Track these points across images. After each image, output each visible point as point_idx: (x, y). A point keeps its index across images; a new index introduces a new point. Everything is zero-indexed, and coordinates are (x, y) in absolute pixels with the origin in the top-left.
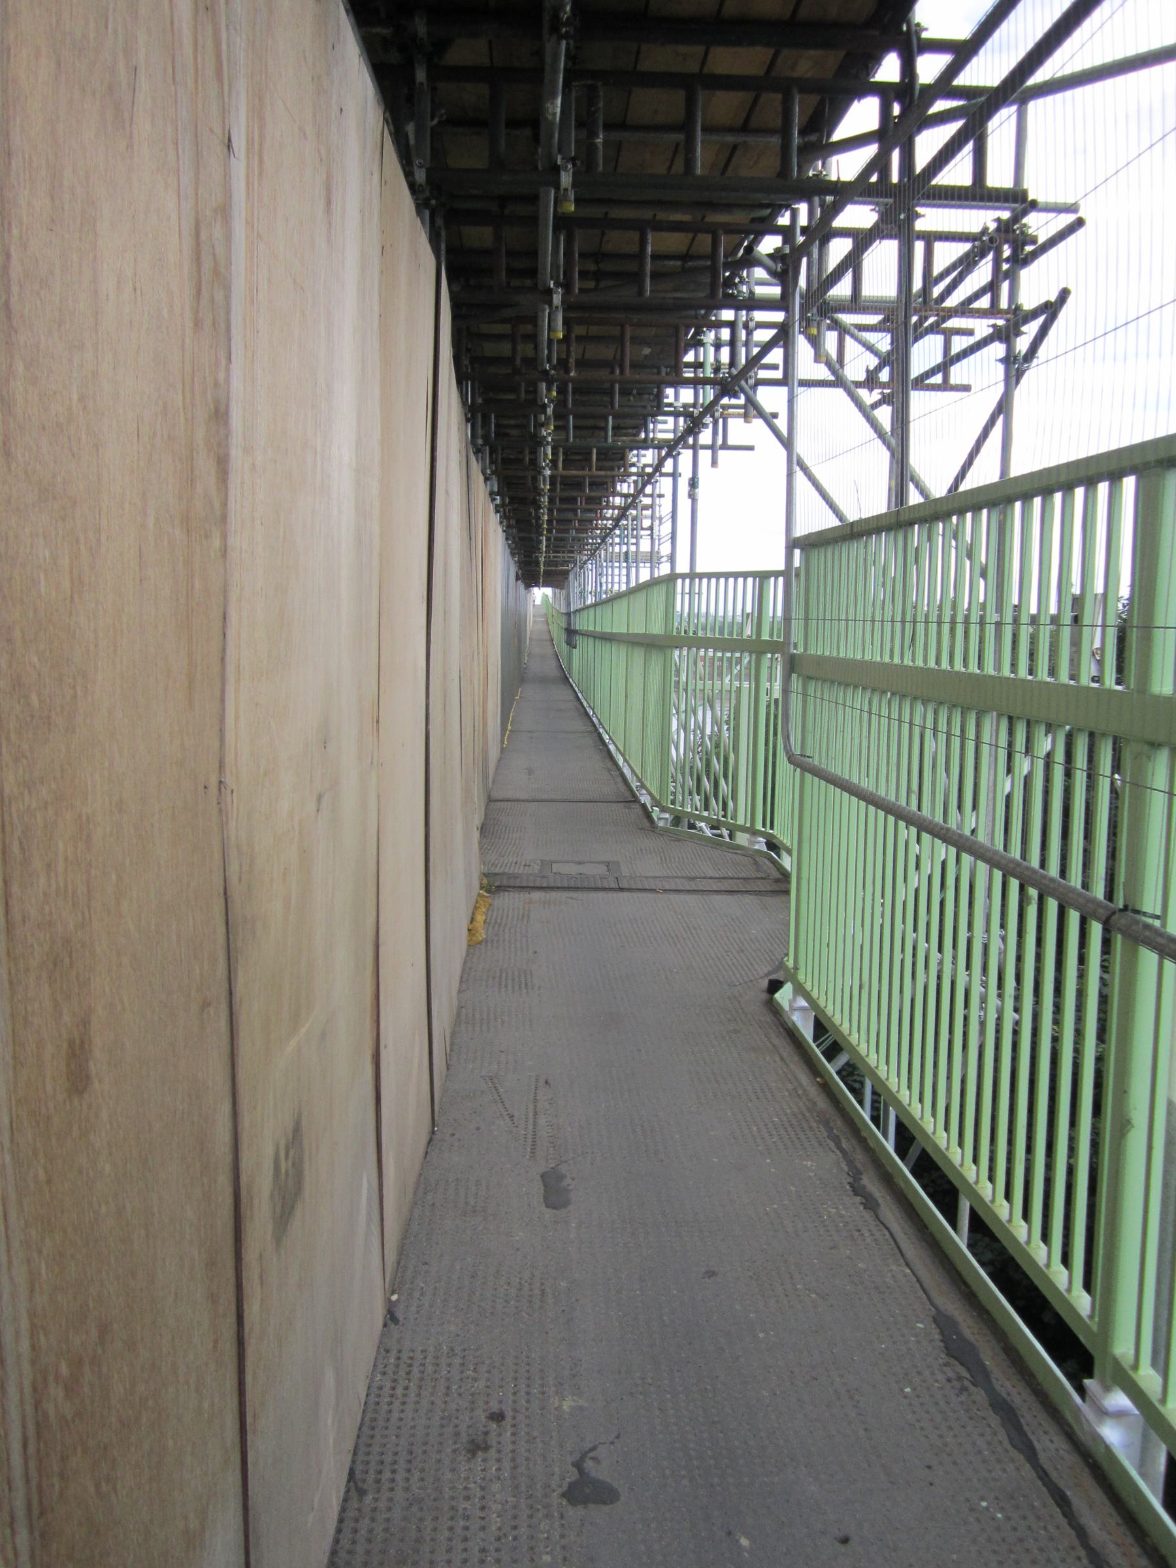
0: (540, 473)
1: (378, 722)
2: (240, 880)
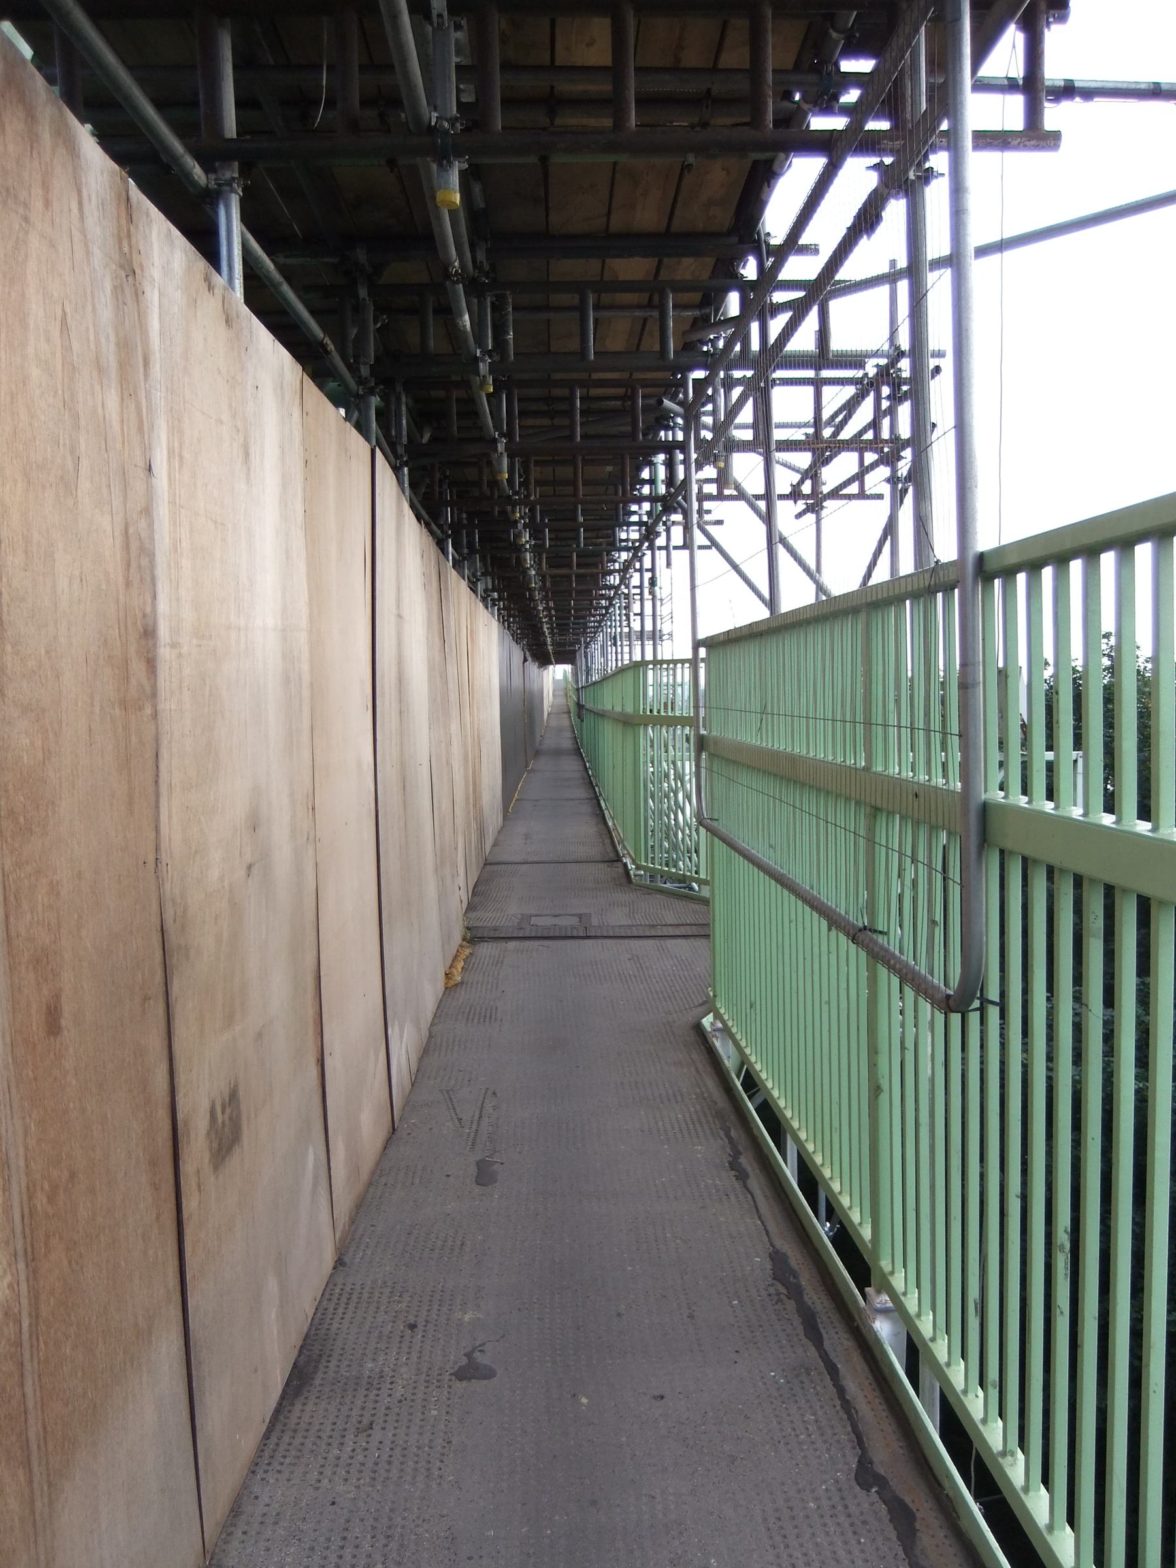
1: (313, 809)
2: (175, 921)
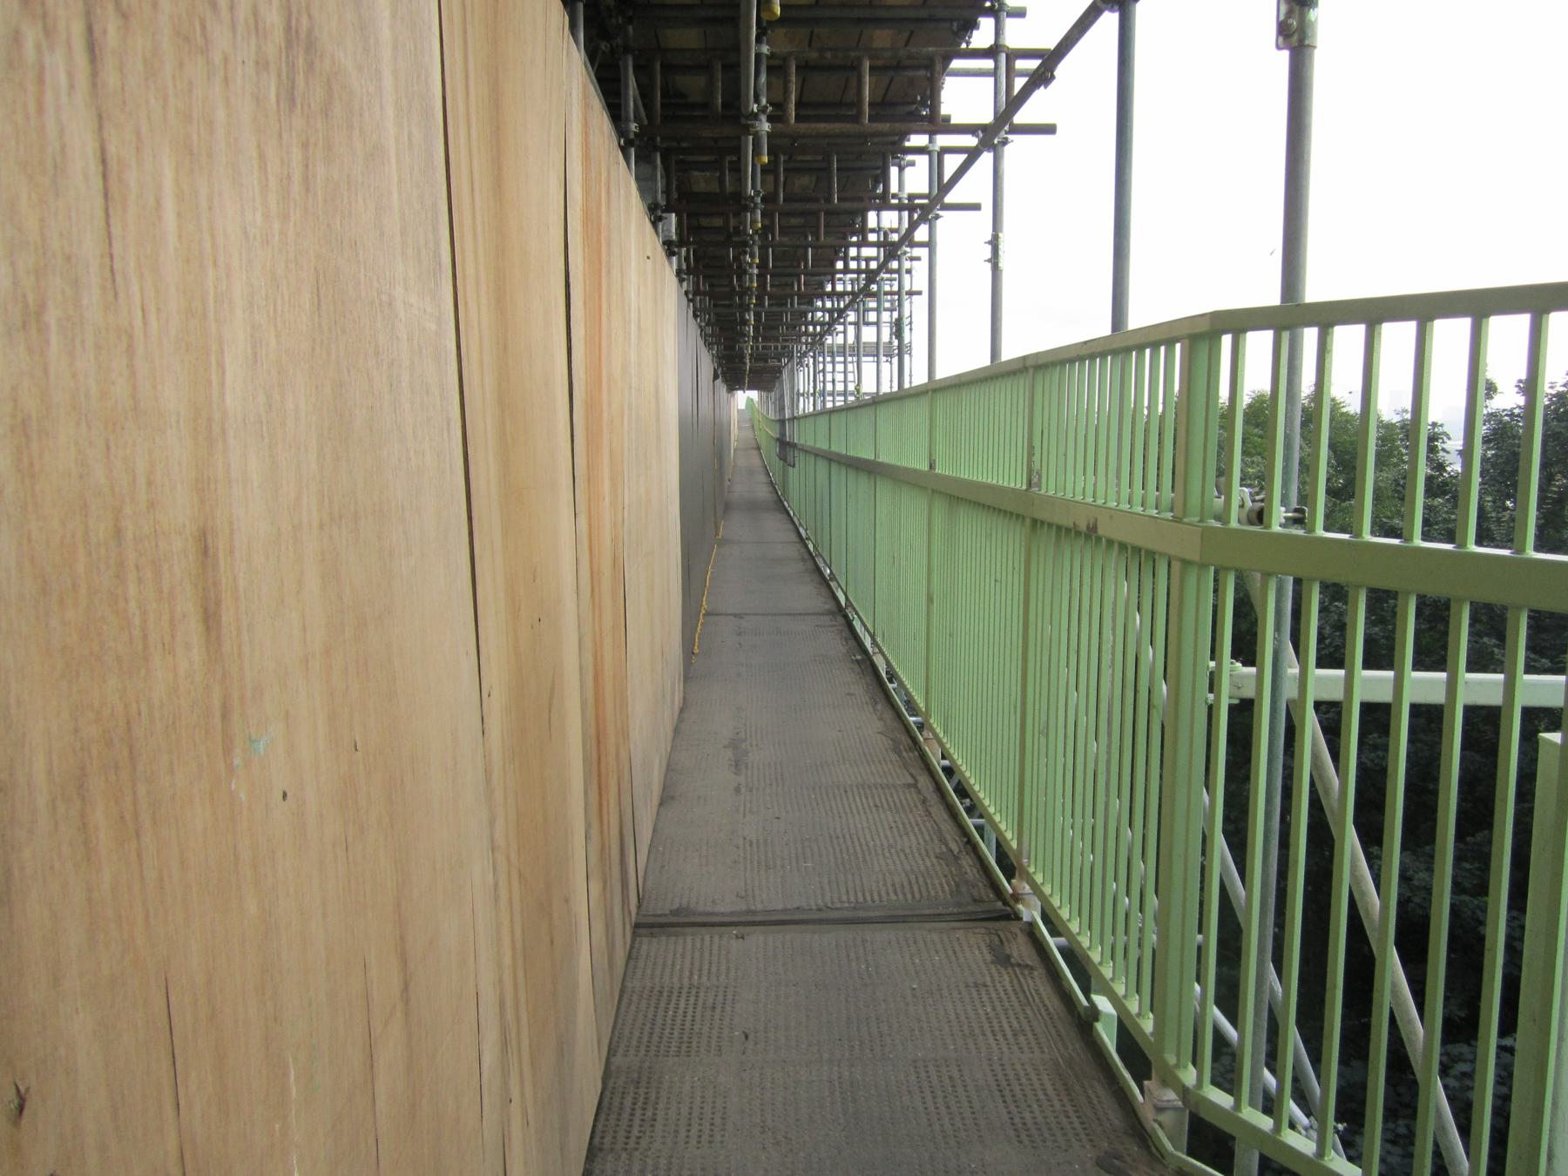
0: (746, 129)
